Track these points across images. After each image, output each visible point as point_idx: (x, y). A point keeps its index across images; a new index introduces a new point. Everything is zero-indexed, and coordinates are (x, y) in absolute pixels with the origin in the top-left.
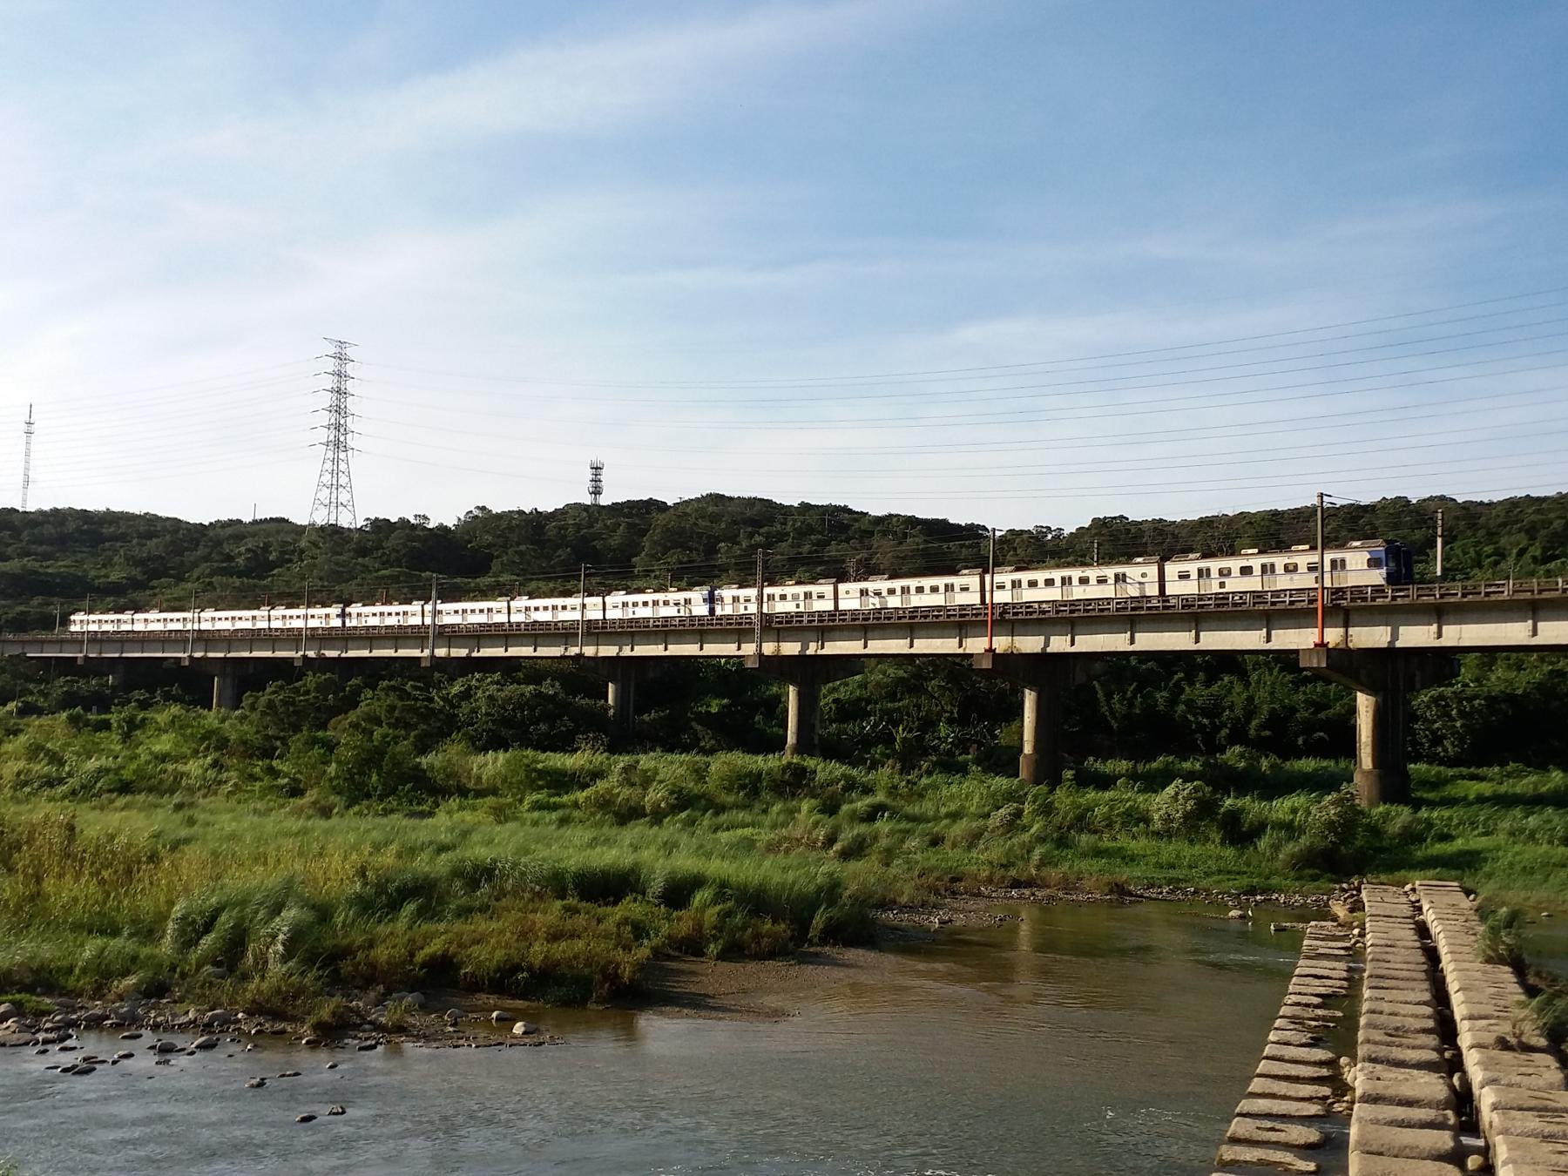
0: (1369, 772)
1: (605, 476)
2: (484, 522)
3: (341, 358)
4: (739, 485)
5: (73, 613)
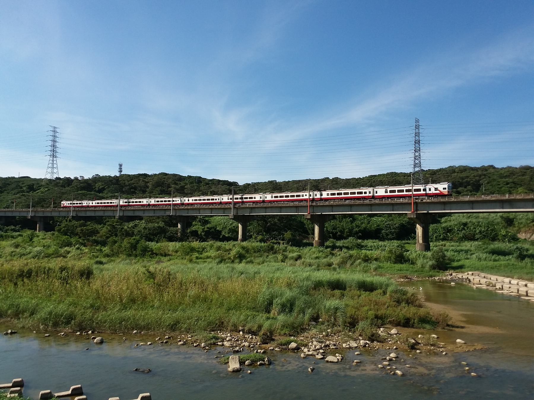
0: (421, 244)
1: (123, 167)
2: (97, 179)
3: (54, 131)
4: (170, 171)
5: (62, 201)
